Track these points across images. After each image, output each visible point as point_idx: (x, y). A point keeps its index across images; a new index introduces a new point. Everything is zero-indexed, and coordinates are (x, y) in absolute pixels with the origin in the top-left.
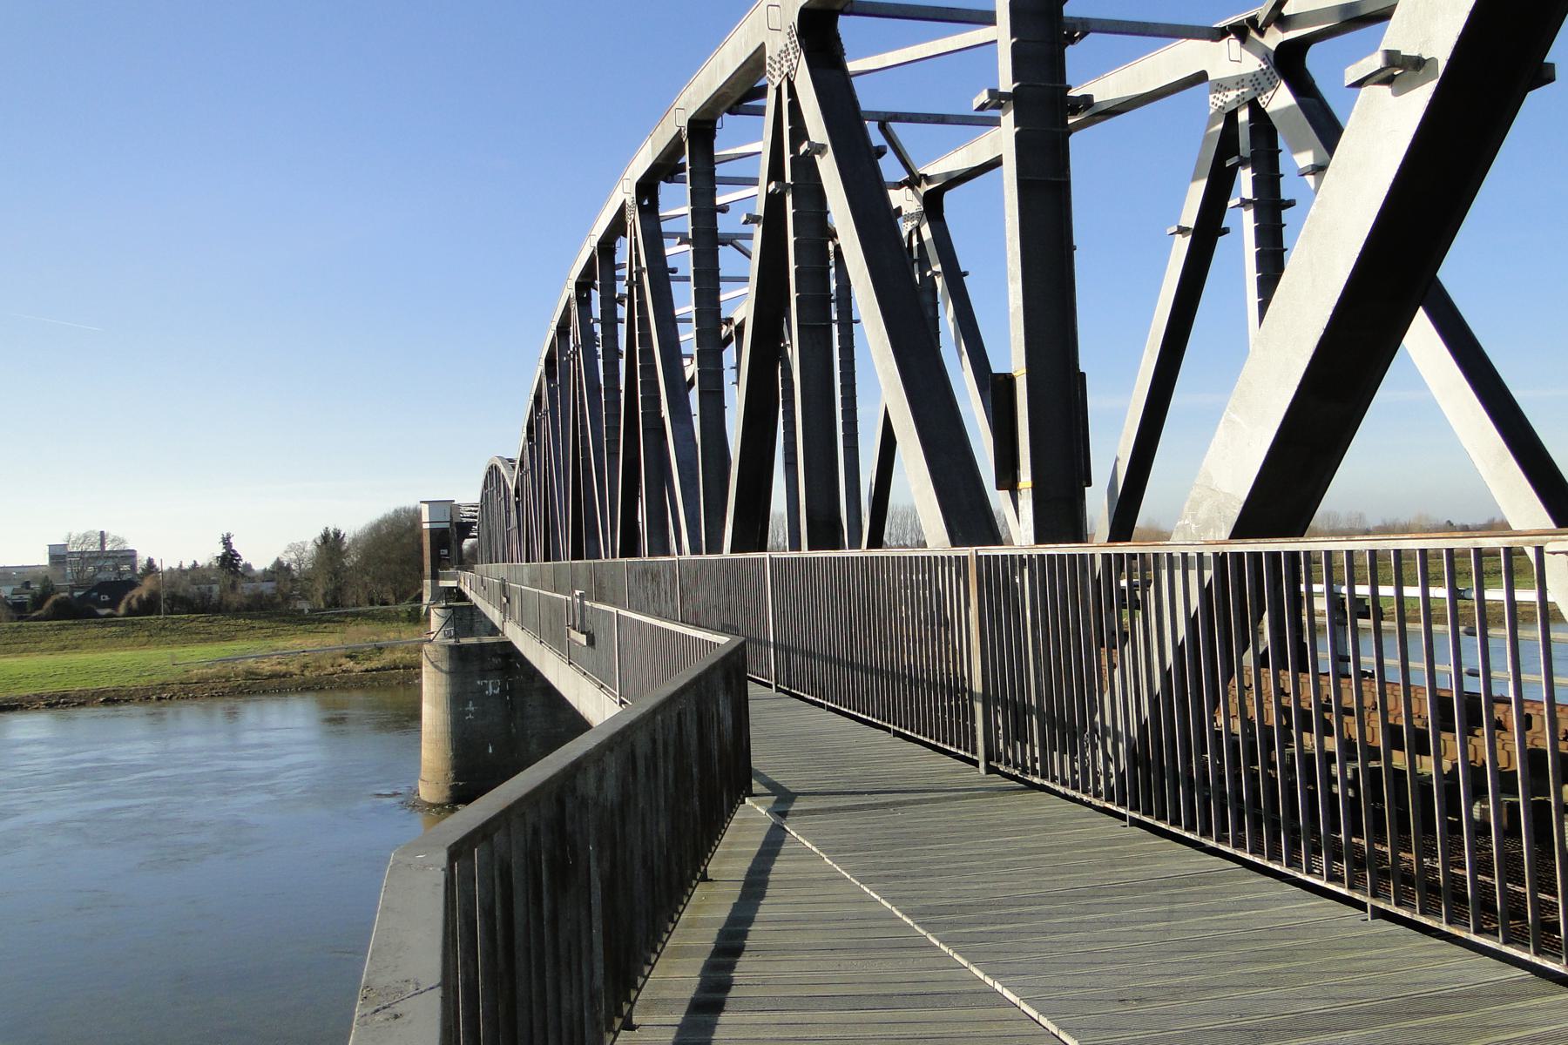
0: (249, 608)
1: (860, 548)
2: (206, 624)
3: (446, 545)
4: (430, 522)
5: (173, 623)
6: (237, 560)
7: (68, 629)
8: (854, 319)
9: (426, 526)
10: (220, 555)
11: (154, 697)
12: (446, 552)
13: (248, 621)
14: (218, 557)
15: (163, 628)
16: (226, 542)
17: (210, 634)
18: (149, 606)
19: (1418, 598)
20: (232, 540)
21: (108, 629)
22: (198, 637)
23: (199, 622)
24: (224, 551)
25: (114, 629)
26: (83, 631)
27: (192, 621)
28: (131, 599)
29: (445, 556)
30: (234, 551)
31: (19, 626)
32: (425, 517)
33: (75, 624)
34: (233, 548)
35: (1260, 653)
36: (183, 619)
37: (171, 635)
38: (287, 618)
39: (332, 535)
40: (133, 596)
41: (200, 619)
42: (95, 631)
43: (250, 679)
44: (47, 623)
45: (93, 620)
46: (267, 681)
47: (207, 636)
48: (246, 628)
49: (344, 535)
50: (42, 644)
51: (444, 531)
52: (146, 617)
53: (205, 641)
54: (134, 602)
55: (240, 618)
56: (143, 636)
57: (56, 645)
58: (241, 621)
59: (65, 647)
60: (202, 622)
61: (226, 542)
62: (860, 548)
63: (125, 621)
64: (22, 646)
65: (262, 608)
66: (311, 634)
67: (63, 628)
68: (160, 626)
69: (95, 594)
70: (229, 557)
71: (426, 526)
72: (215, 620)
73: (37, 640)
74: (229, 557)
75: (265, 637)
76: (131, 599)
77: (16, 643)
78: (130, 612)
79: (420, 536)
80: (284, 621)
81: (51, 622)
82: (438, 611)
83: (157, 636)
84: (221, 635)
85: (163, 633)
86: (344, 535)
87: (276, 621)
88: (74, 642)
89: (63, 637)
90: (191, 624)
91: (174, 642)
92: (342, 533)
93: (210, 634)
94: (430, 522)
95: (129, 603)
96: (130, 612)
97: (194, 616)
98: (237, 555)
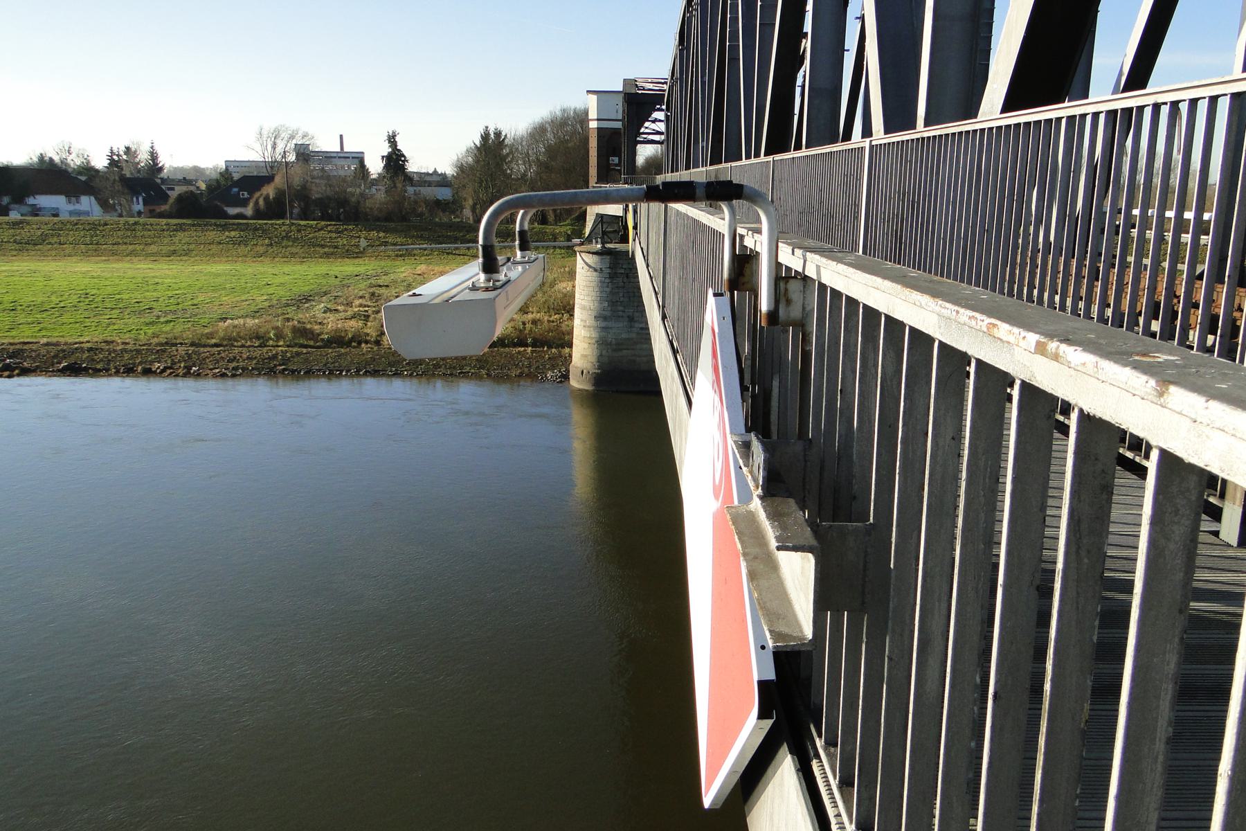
0: (388, 218)
1: (742, 160)
2: (334, 235)
3: (616, 152)
4: (598, 120)
5: (299, 231)
6: (402, 161)
7: (184, 231)
8: (845, 48)
9: (593, 125)
10: (386, 154)
11: (140, 368)
12: (616, 160)
13: (381, 234)
14: (383, 157)
15: (287, 237)
16: (392, 140)
17: (336, 247)
18: (275, 209)
19: (1171, 218)
20: (397, 139)
21: (227, 233)
22: (322, 251)
23: (325, 231)
24: (390, 150)
25: (233, 233)
26: (199, 234)
27: (319, 230)
28: (259, 197)
29: (616, 165)
30: (399, 150)
31: (136, 223)
32: (593, 114)
33: (194, 225)
34: (398, 148)
35: (1196, 274)
36: (311, 227)
37: (292, 246)
38: (426, 234)
39: (492, 136)
40: (261, 195)
41: (329, 228)
42: (212, 235)
43: (296, 345)
44: (164, 221)
45: (213, 221)
46: (319, 352)
47: (332, 250)
48: (378, 243)
49: (506, 135)
50: (153, 246)
51: (615, 132)
52: (270, 222)
53: (327, 256)
54: (261, 202)
55: (373, 230)
56: (262, 245)
57: (165, 249)
58: (374, 234)
59: (174, 252)
60: (330, 232)
61: (392, 140)
62: (742, 160)
63: (247, 224)
64: (131, 247)
65: (404, 219)
66: (450, 256)
67: (181, 228)
68: (284, 234)
69: (235, 190)
70: (394, 157)
71: (593, 125)
72: (346, 229)
73: (149, 241)
74: (394, 157)
75: (397, 256)
76: (259, 197)
77: (126, 244)
78: (258, 214)
79: (586, 140)
80: (421, 237)
81: (169, 220)
82: (591, 259)
83: (280, 246)
84: (347, 251)
85: (285, 243)
86: (506, 135)
87: (412, 237)
88: (185, 247)
89: (176, 240)
90: (317, 234)
91: (293, 255)
92: (503, 134)
93: (336, 247)
94: (598, 120)
95: (257, 203)
96: (258, 214)
97: (323, 223)
98: (403, 156)
